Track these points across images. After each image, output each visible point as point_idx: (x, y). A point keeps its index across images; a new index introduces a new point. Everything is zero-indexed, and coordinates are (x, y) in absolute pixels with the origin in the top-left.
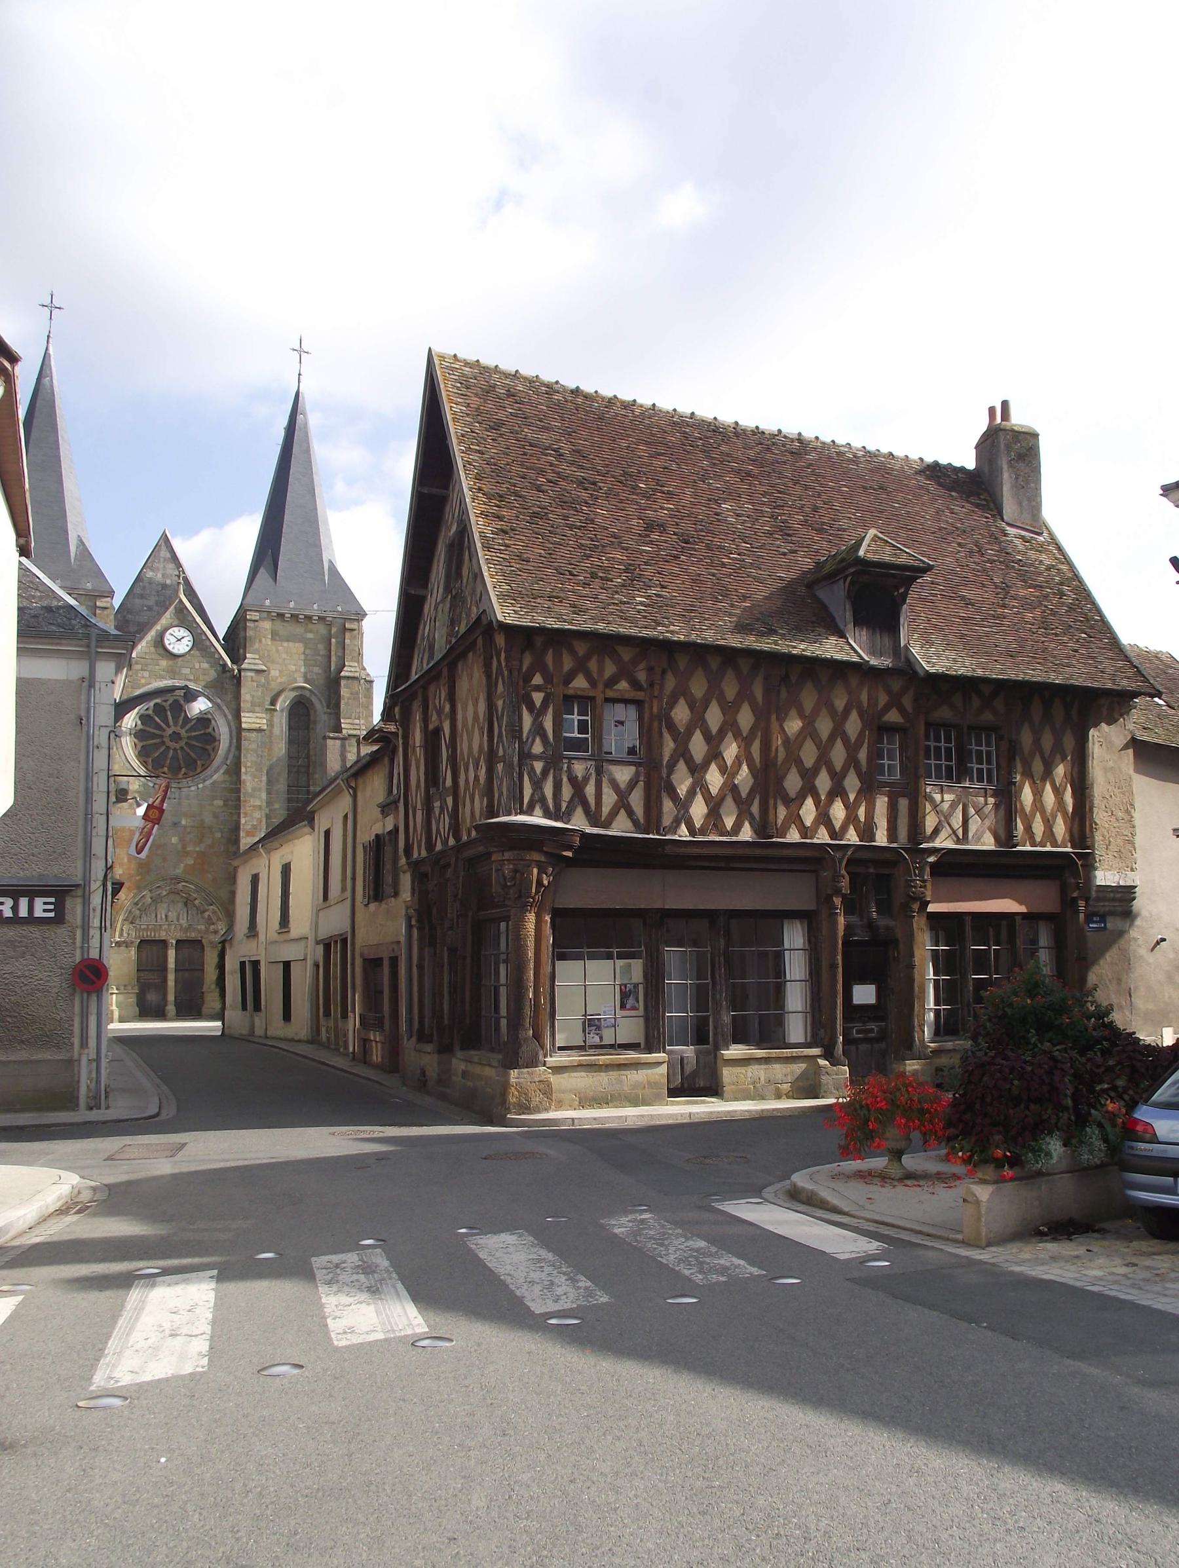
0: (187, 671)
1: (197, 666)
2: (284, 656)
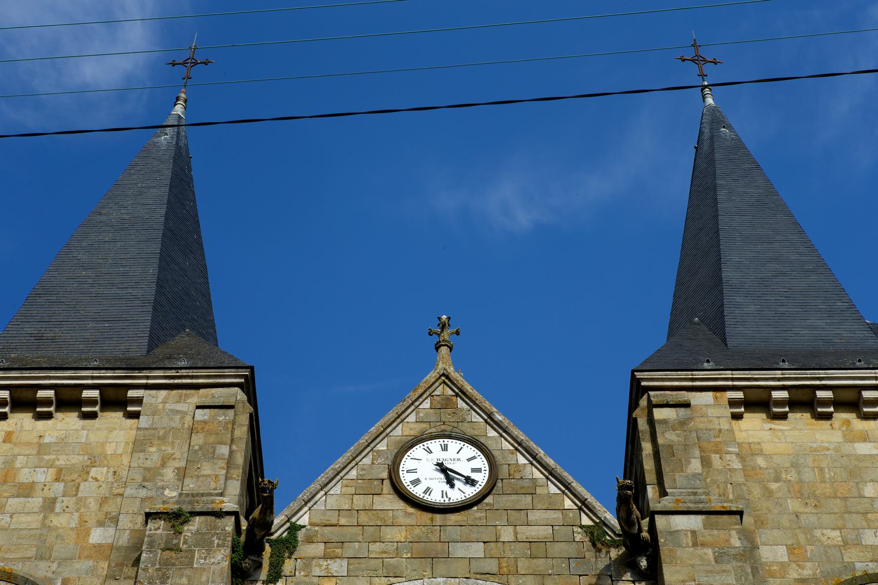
0: (477, 550)
1: (507, 534)
2: (793, 505)
